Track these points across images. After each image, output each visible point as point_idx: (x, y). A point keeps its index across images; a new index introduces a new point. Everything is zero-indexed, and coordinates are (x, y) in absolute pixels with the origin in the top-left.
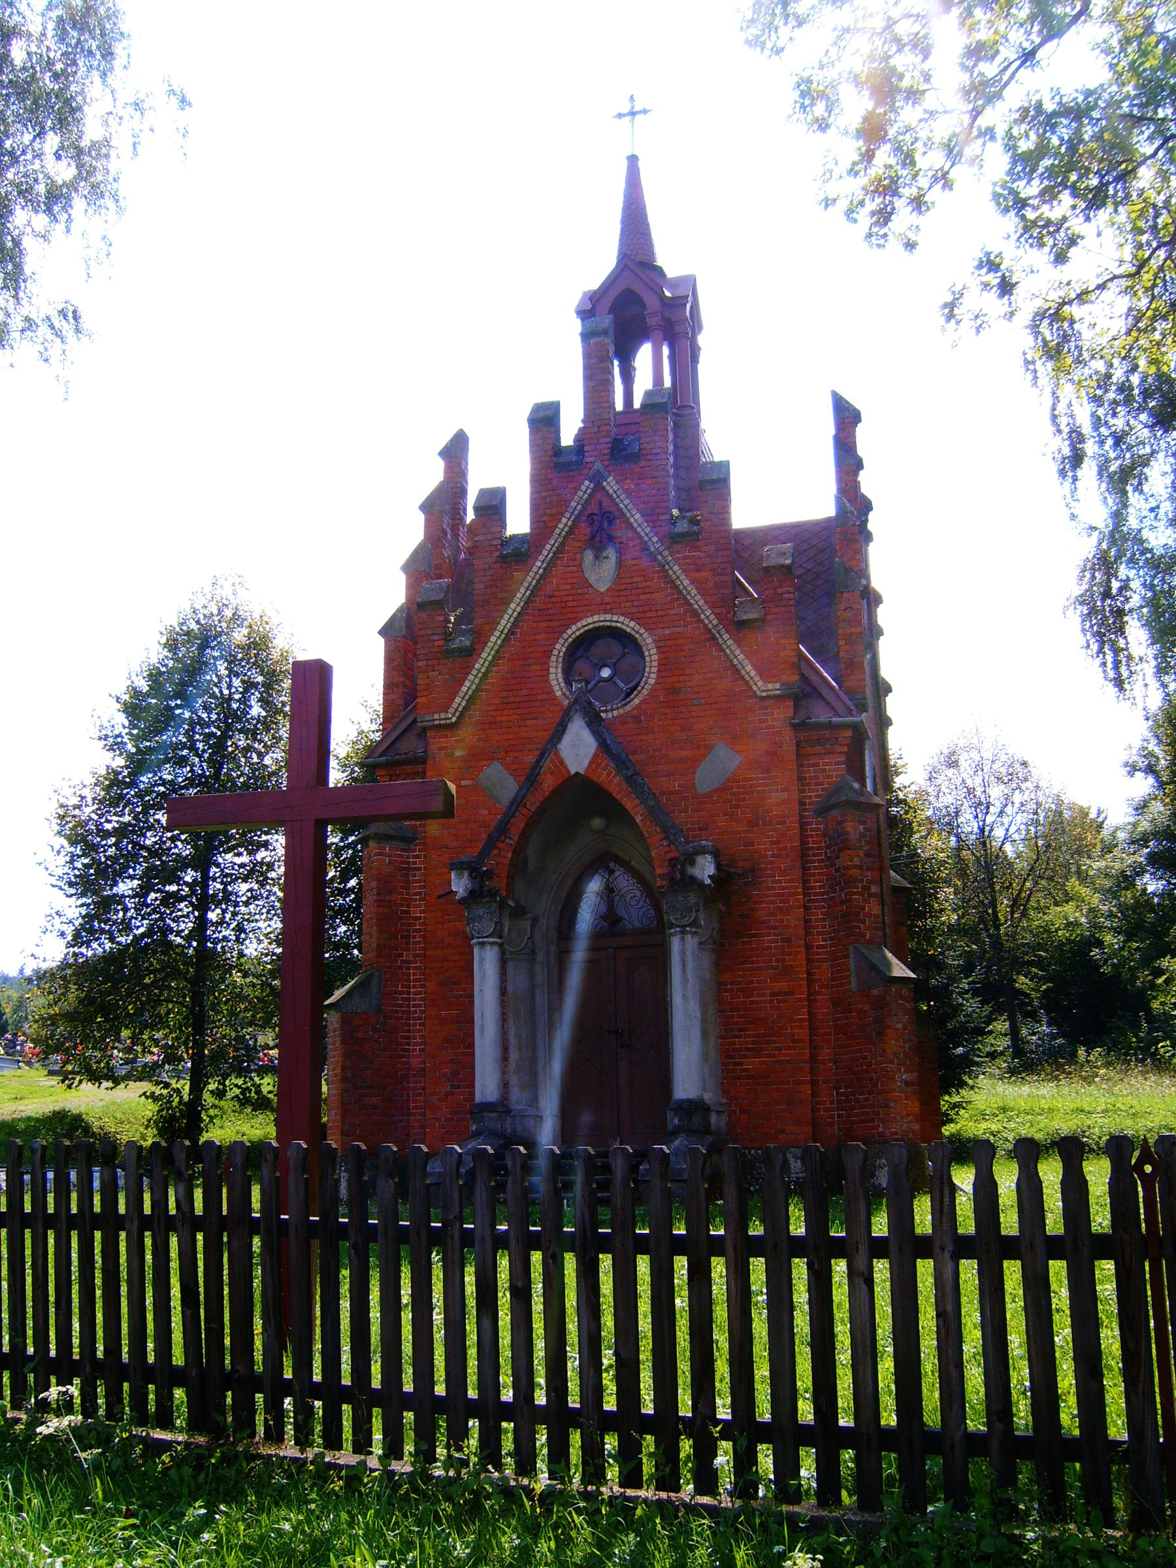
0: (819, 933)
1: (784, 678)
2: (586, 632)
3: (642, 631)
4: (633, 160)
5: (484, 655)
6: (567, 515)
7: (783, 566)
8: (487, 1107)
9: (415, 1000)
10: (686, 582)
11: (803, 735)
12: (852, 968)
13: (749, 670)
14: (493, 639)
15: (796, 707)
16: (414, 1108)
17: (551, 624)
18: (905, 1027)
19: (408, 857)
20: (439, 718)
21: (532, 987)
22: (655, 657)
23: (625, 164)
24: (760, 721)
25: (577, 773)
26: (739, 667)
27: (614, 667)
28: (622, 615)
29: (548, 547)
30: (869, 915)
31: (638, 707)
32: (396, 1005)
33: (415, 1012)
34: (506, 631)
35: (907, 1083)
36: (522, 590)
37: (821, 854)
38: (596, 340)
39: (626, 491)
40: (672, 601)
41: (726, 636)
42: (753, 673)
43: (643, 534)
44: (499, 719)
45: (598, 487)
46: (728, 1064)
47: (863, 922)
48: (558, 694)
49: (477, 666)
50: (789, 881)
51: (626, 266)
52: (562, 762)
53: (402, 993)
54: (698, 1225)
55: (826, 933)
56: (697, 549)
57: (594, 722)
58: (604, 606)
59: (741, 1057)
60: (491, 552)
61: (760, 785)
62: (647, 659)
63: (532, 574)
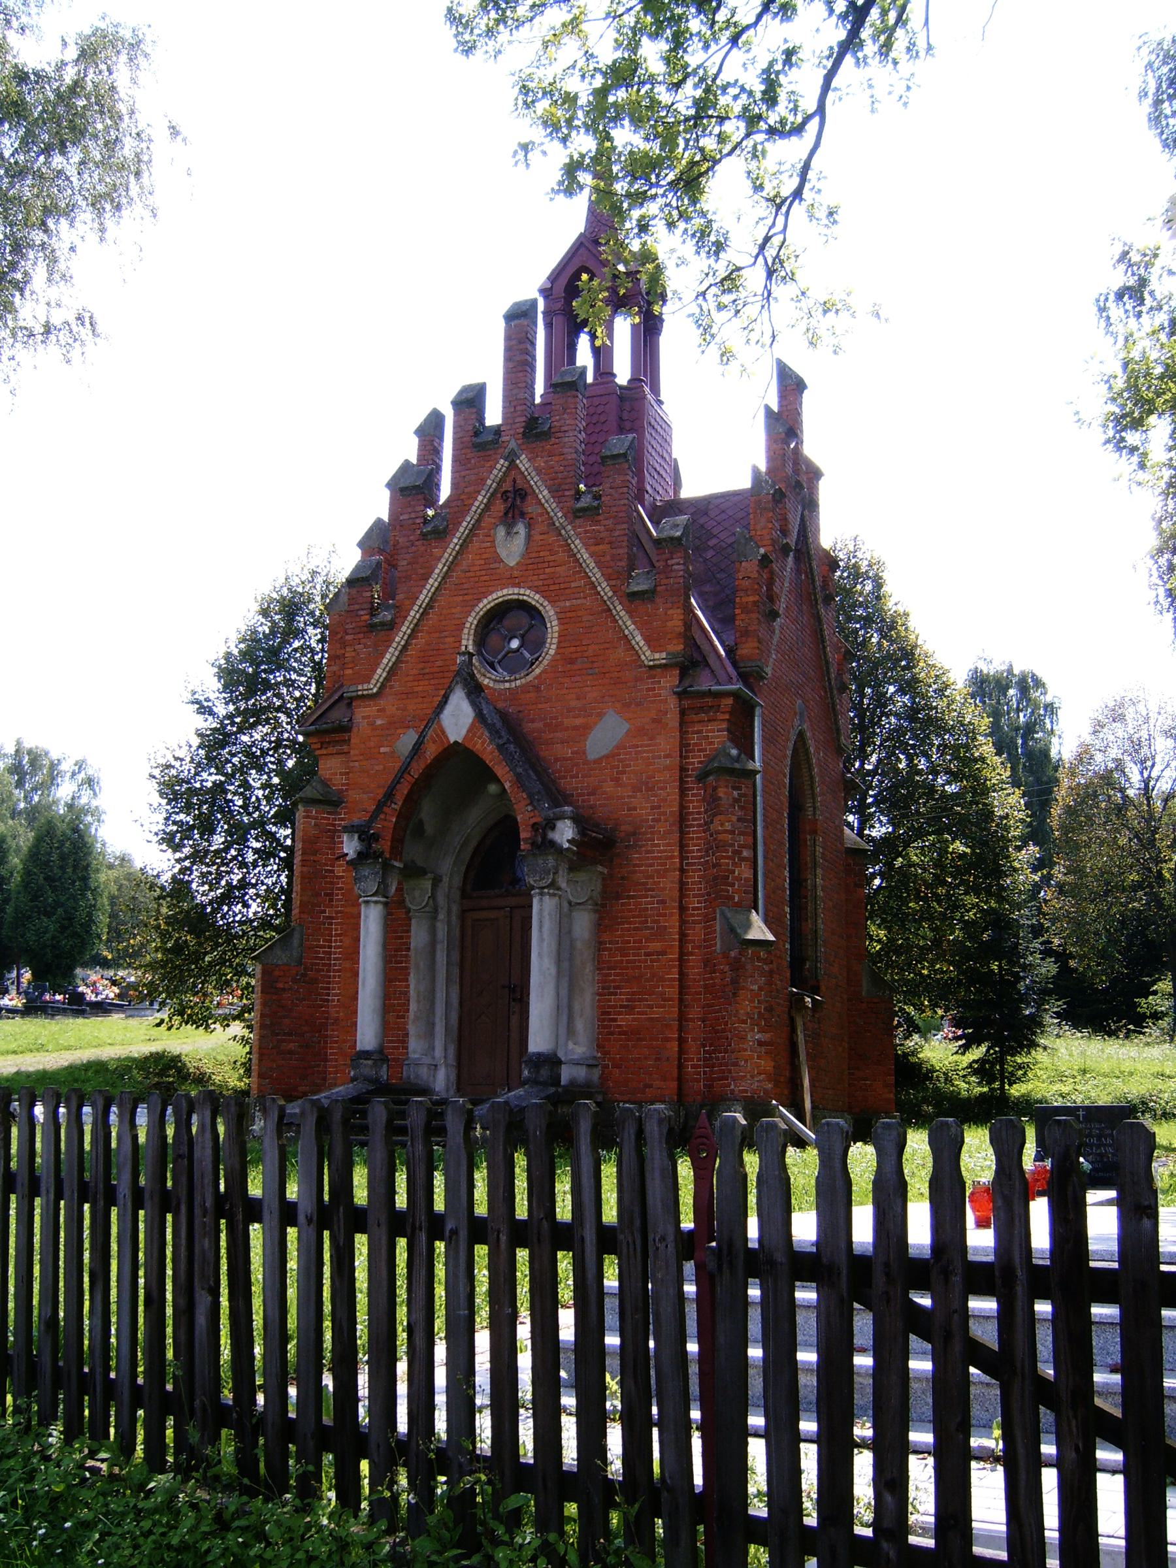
1: (671, 648)
2: (496, 605)
3: (546, 603)
5: (404, 629)
6: (483, 493)
7: (672, 539)
8: (366, 1054)
10: (586, 556)
11: (686, 703)
12: (718, 928)
13: (639, 640)
14: (412, 613)
15: (682, 676)
18: (760, 989)
21: (433, 943)
22: (556, 629)
24: (649, 690)
25: (456, 743)
26: (630, 637)
27: (523, 638)
28: (529, 588)
29: (465, 524)
30: (739, 879)
31: (538, 677)
32: (317, 958)
35: (760, 1043)
36: (440, 566)
37: (699, 819)
38: (516, 322)
39: (536, 469)
40: (575, 573)
41: (619, 608)
42: (642, 643)
44: (416, 689)
45: (512, 466)
46: (604, 1020)
47: (733, 885)
49: (397, 639)
50: (668, 845)
51: (582, 243)
52: (443, 732)
53: (324, 947)
55: (702, 895)
56: (598, 522)
57: (475, 691)
58: (513, 580)
61: (645, 752)
63: (449, 550)
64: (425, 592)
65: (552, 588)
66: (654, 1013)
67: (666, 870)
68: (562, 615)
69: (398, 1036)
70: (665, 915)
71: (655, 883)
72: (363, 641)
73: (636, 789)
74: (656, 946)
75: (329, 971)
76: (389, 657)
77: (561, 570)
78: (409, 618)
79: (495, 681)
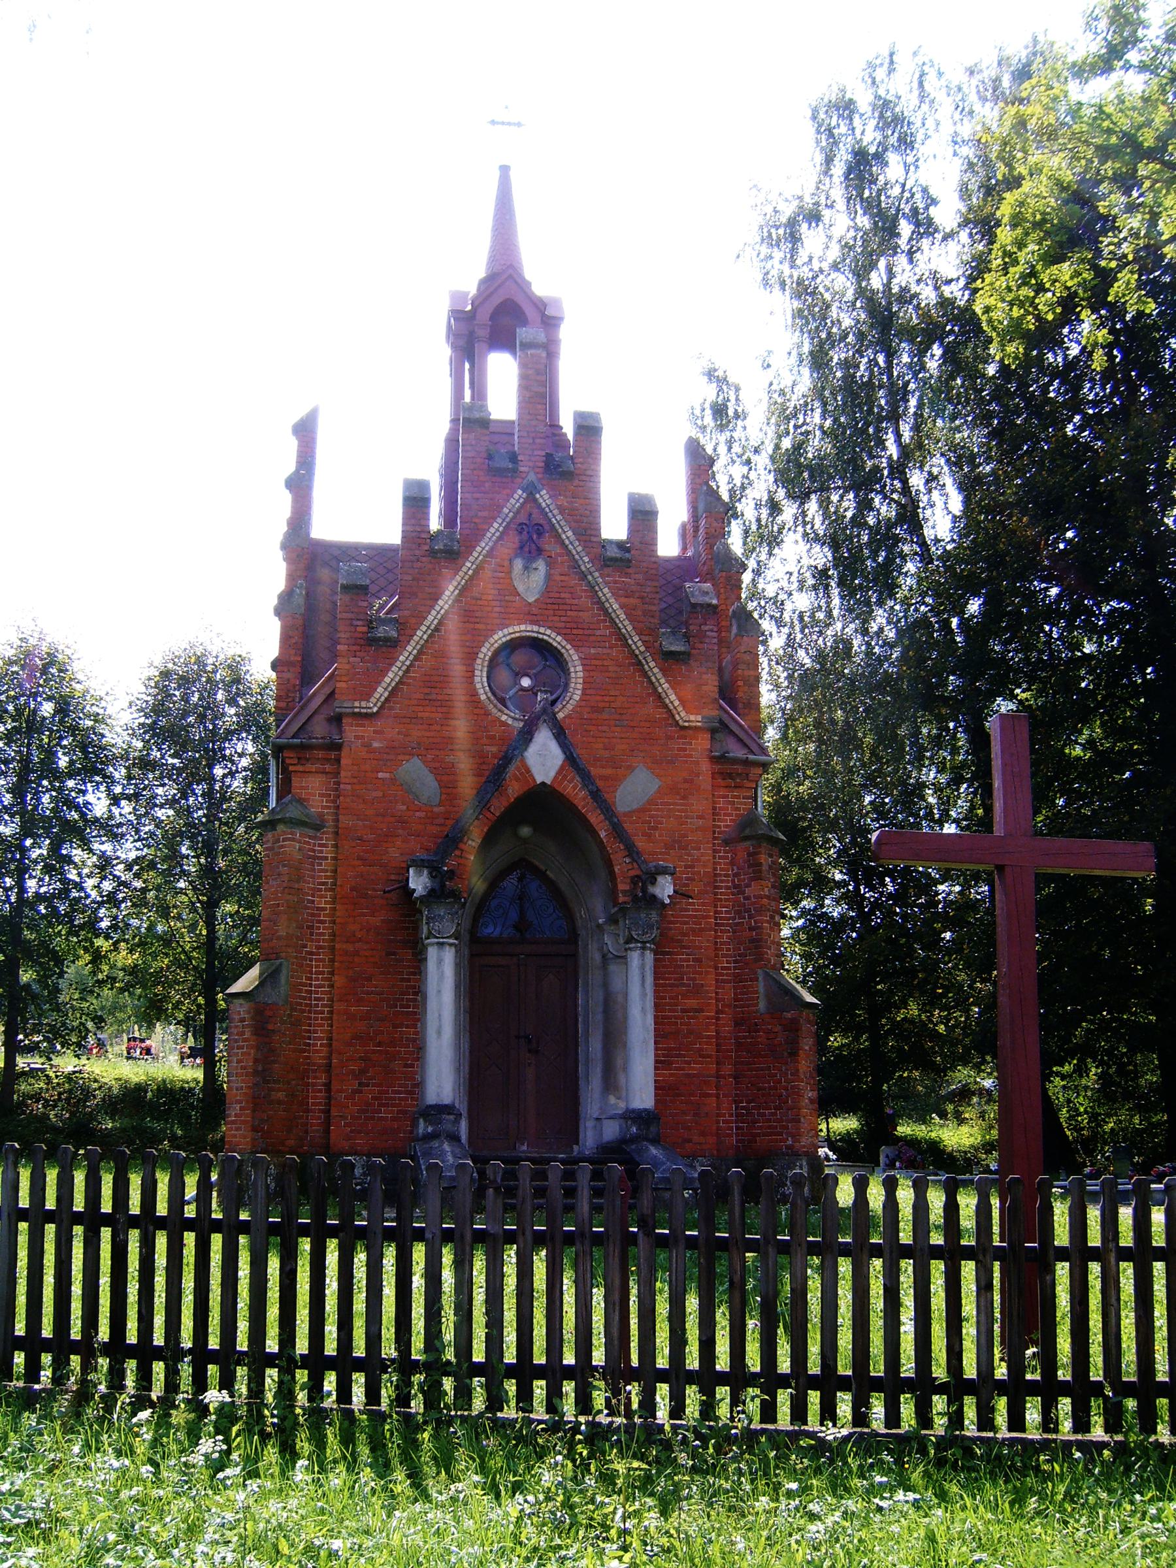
0: (724, 956)
3: (568, 647)
4: (505, 170)
5: (409, 648)
6: (499, 520)
9: (317, 992)
10: (616, 606)
14: (419, 633)
19: (314, 845)
20: (360, 706)
22: (581, 674)
23: (497, 173)
24: (679, 749)
25: (543, 784)
26: (663, 695)
28: (549, 628)
33: (317, 1006)
34: (433, 627)
36: (451, 588)
39: (559, 507)
41: (652, 664)
43: (574, 552)
44: (420, 715)
45: (531, 499)
48: (483, 697)
49: (402, 658)
50: (703, 904)
52: (528, 770)
53: (305, 985)
54: (319, 1215)
56: (627, 575)
60: (419, 545)
62: (573, 675)
63: (461, 573)
64: (434, 613)
65: (575, 632)
66: (693, 1069)
67: (702, 930)
68: (586, 662)
69: (406, 1086)
70: (700, 973)
71: (691, 941)
73: (669, 847)
74: (692, 1003)
75: (310, 1012)
76: (391, 677)
77: (585, 616)
79: (514, 719)
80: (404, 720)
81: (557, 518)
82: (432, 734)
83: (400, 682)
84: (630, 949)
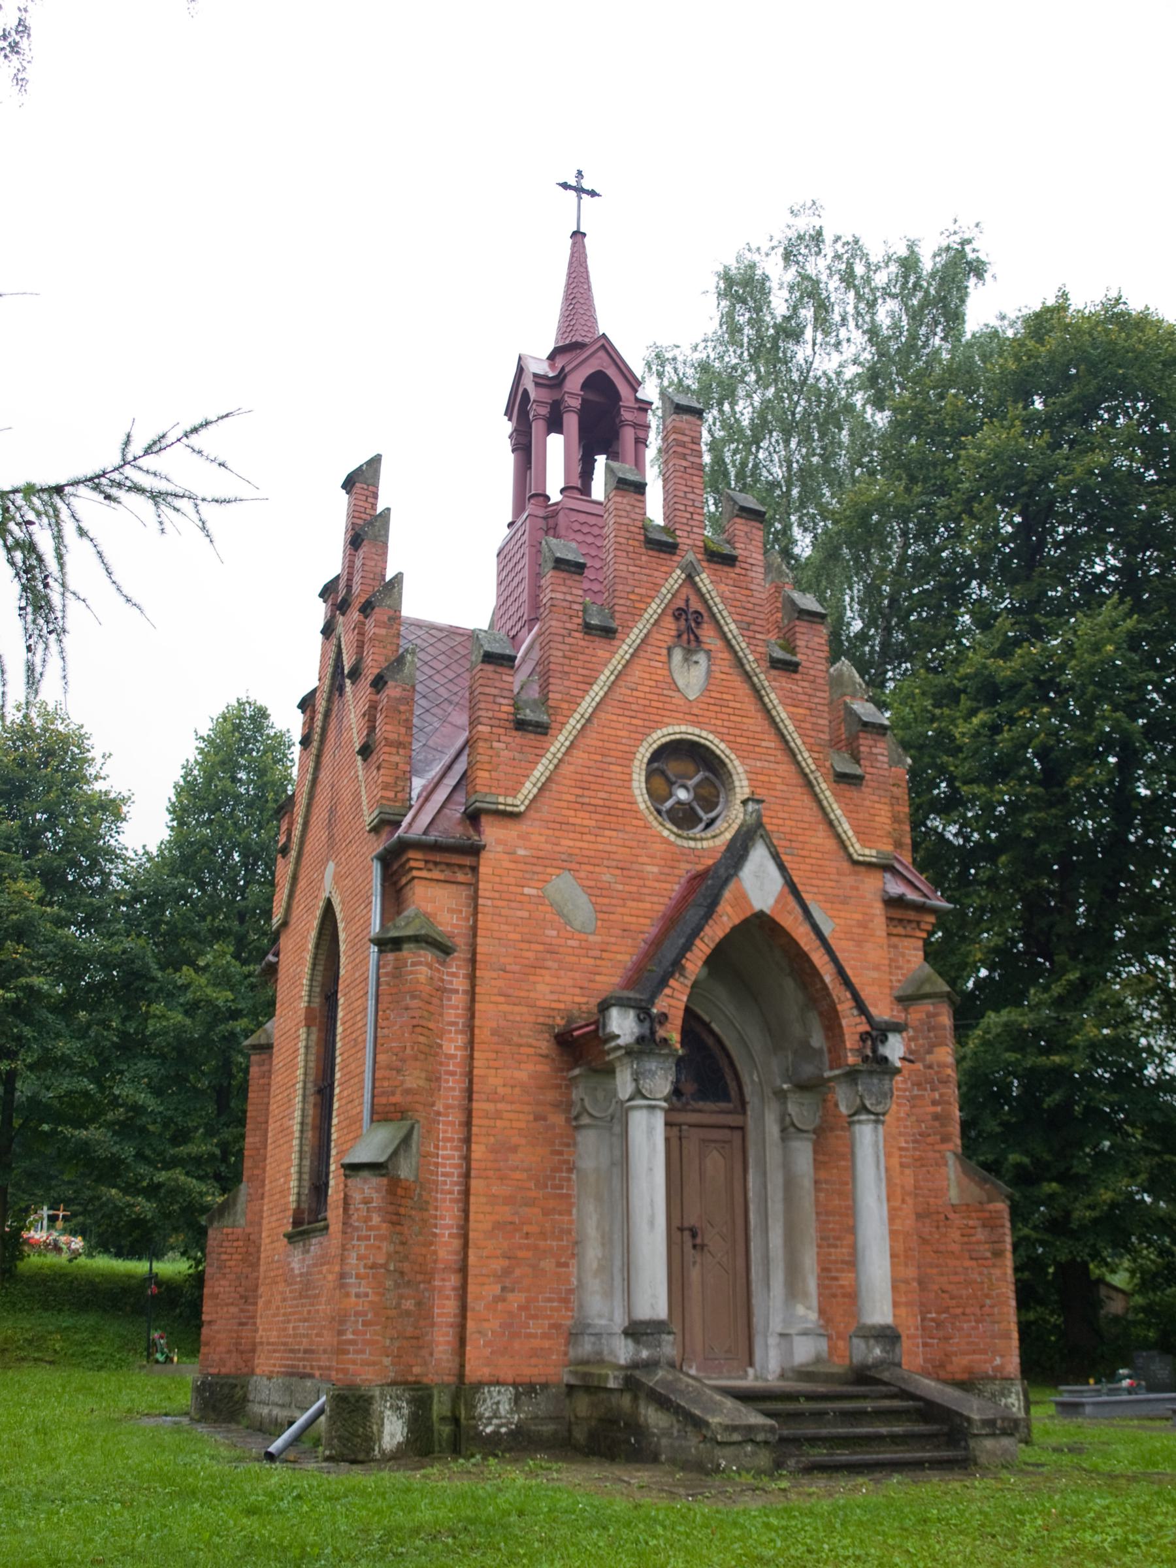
3: (733, 756)
5: (561, 738)
6: (657, 601)
10: (784, 715)
14: (572, 721)
16: (440, 1315)
17: (634, 721)
20: (505, 802)
21: (876, 1144)
36: (607, 673)
42: (850, 833)
44: (572, 820)
49: (553, 749)
59: (838, 1270)
63: (618, 657)
64: (588, 699)
65: (739, 740)
68: (753, 776)
72: (503, 738)
76: (540, 771)
78: (569, 727)
80: (551, 825)
81: (718, 606)
82: (585, 845)
83: (549, 779)
84: (859, 1122)
